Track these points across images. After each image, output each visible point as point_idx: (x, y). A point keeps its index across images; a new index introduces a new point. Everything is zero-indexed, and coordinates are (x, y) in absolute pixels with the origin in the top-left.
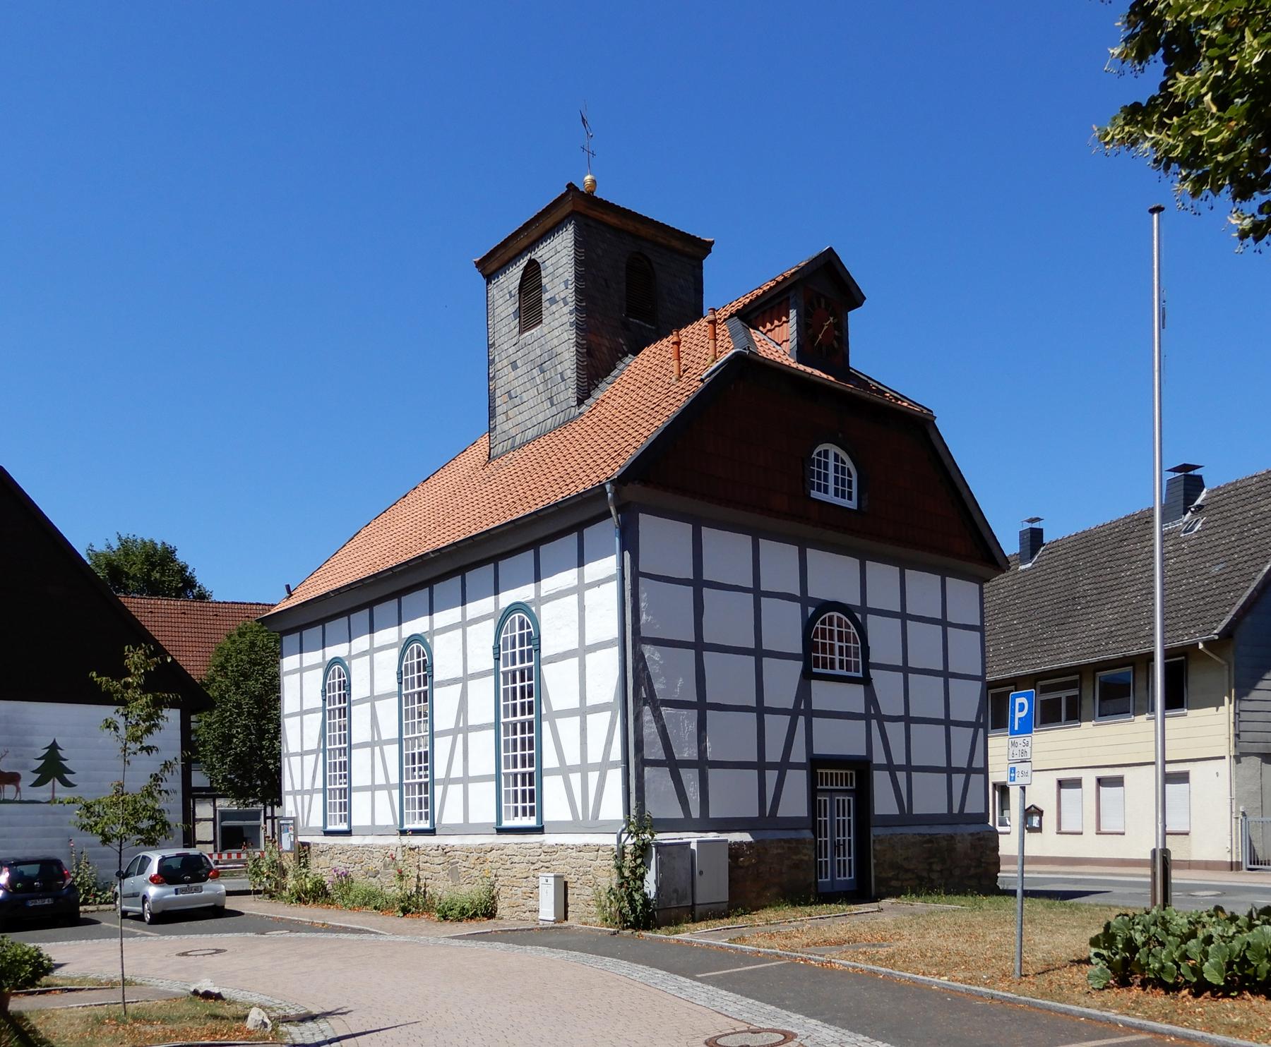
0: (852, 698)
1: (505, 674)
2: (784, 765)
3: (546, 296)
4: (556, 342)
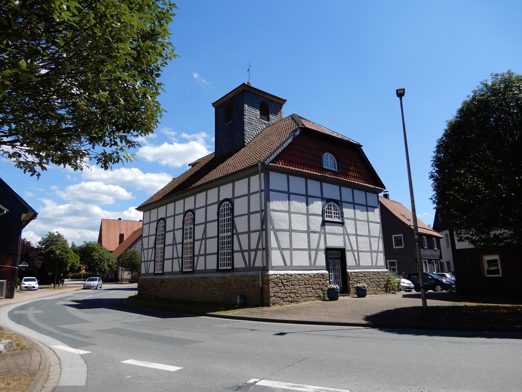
0: (338, 229)
2: (256, 250)
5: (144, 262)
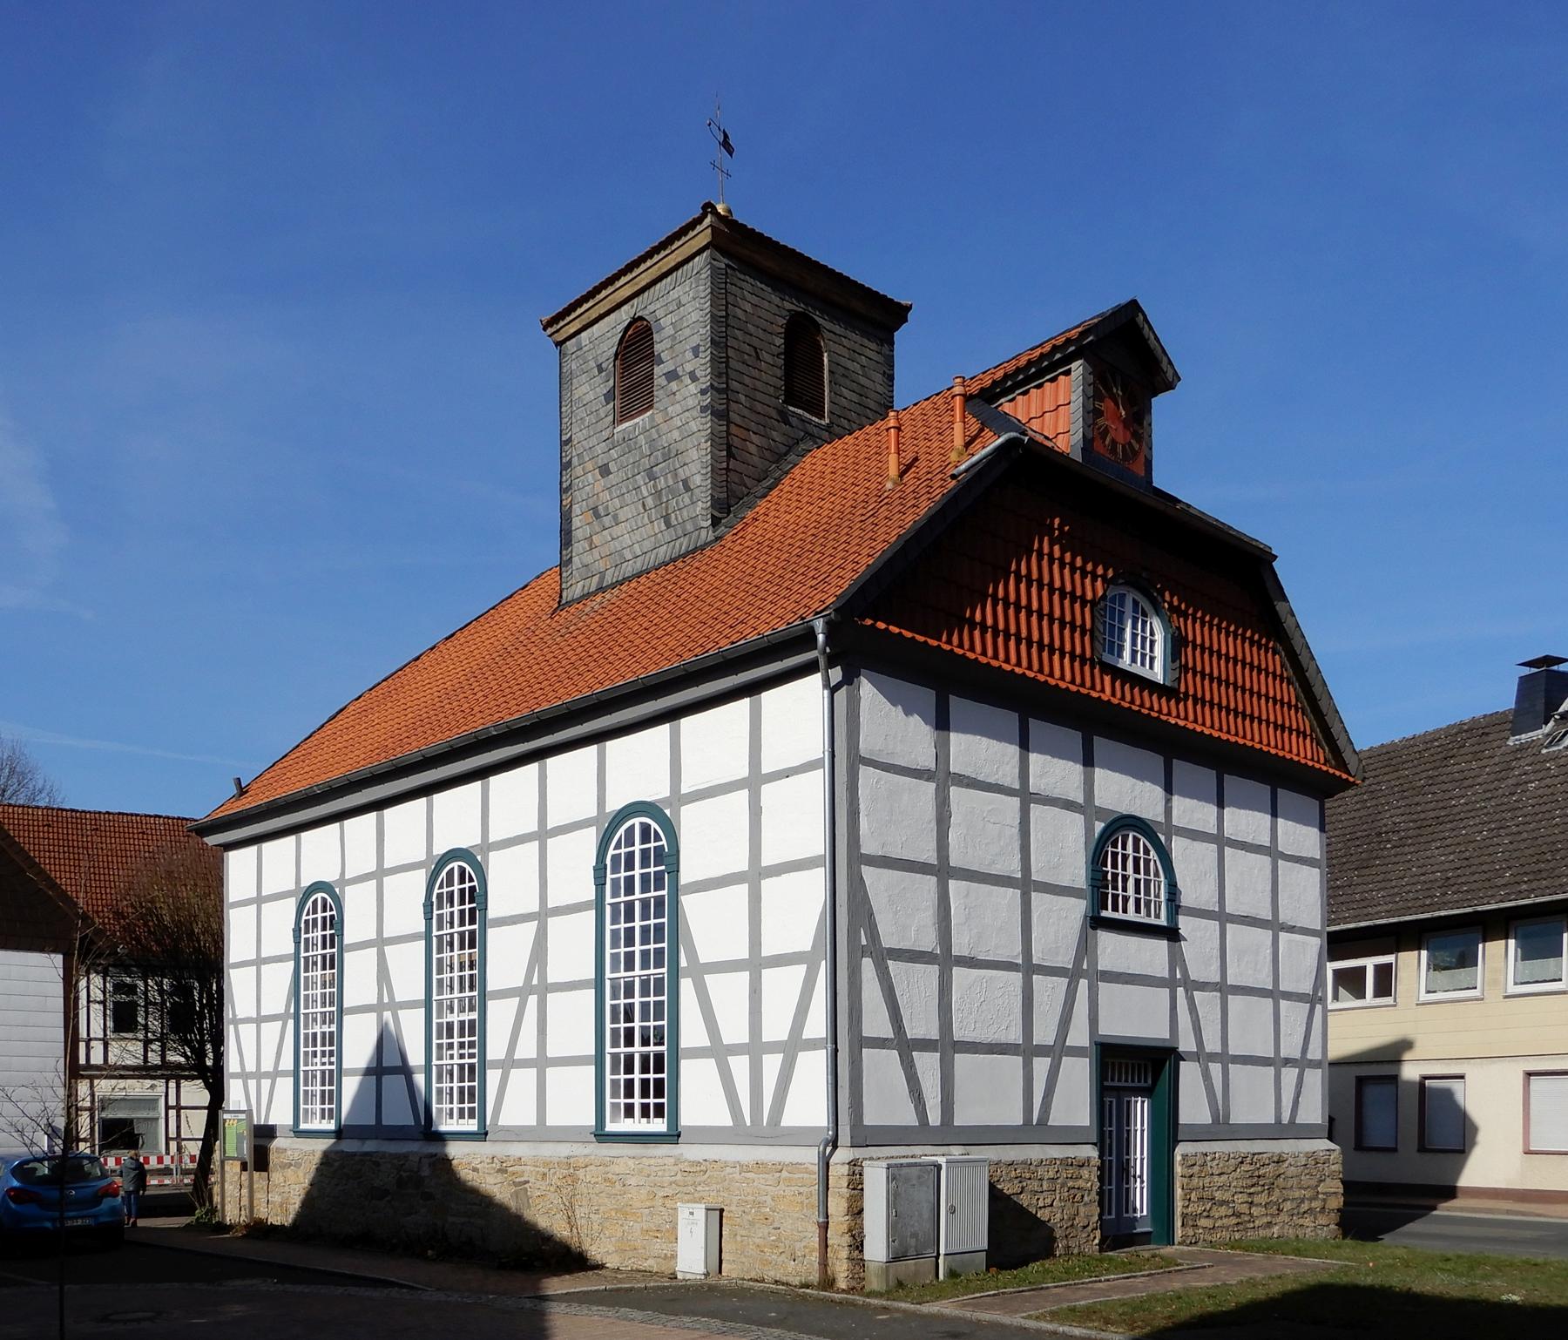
0: (1150, 955)
1: (440, 938)
2: (793, 1046)
3: (658, 370)
4: (676, 435)
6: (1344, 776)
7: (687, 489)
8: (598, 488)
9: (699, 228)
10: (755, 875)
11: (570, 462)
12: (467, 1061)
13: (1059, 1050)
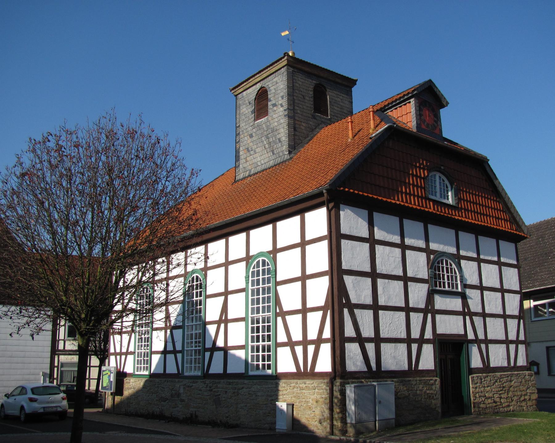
0: (456, 304)
2: (318, 342)
3: (269, 103)
4: (276, 124)
5: (116, 354)
6: (523, 235)
7: (280, 141)
8: (249, 142)
9: (283, 60)
10: (304, 278)
11: (239, 133)
12: (198, 348)
13: (421, 341)
